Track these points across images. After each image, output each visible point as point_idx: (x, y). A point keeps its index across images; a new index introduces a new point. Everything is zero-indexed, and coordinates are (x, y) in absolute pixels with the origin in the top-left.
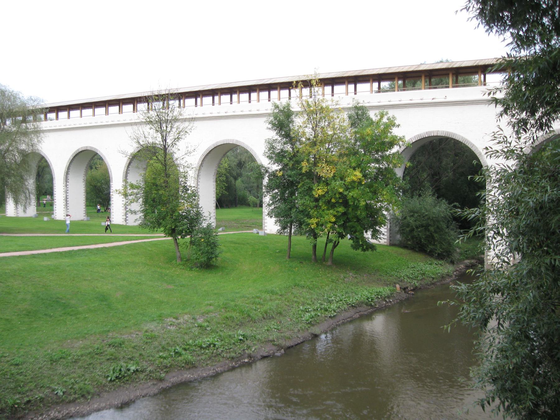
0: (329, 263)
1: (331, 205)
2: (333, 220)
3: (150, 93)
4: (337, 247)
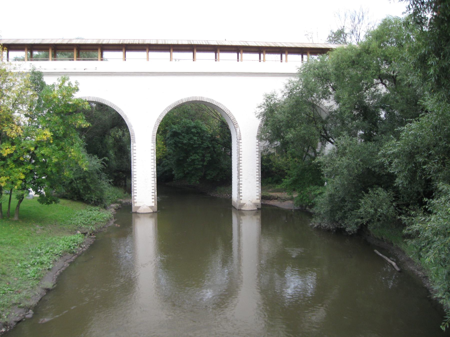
0: (16, 218)
1: (19, 163)
2: (23, 177)
3: (137, 41)
4: (22, 203)
